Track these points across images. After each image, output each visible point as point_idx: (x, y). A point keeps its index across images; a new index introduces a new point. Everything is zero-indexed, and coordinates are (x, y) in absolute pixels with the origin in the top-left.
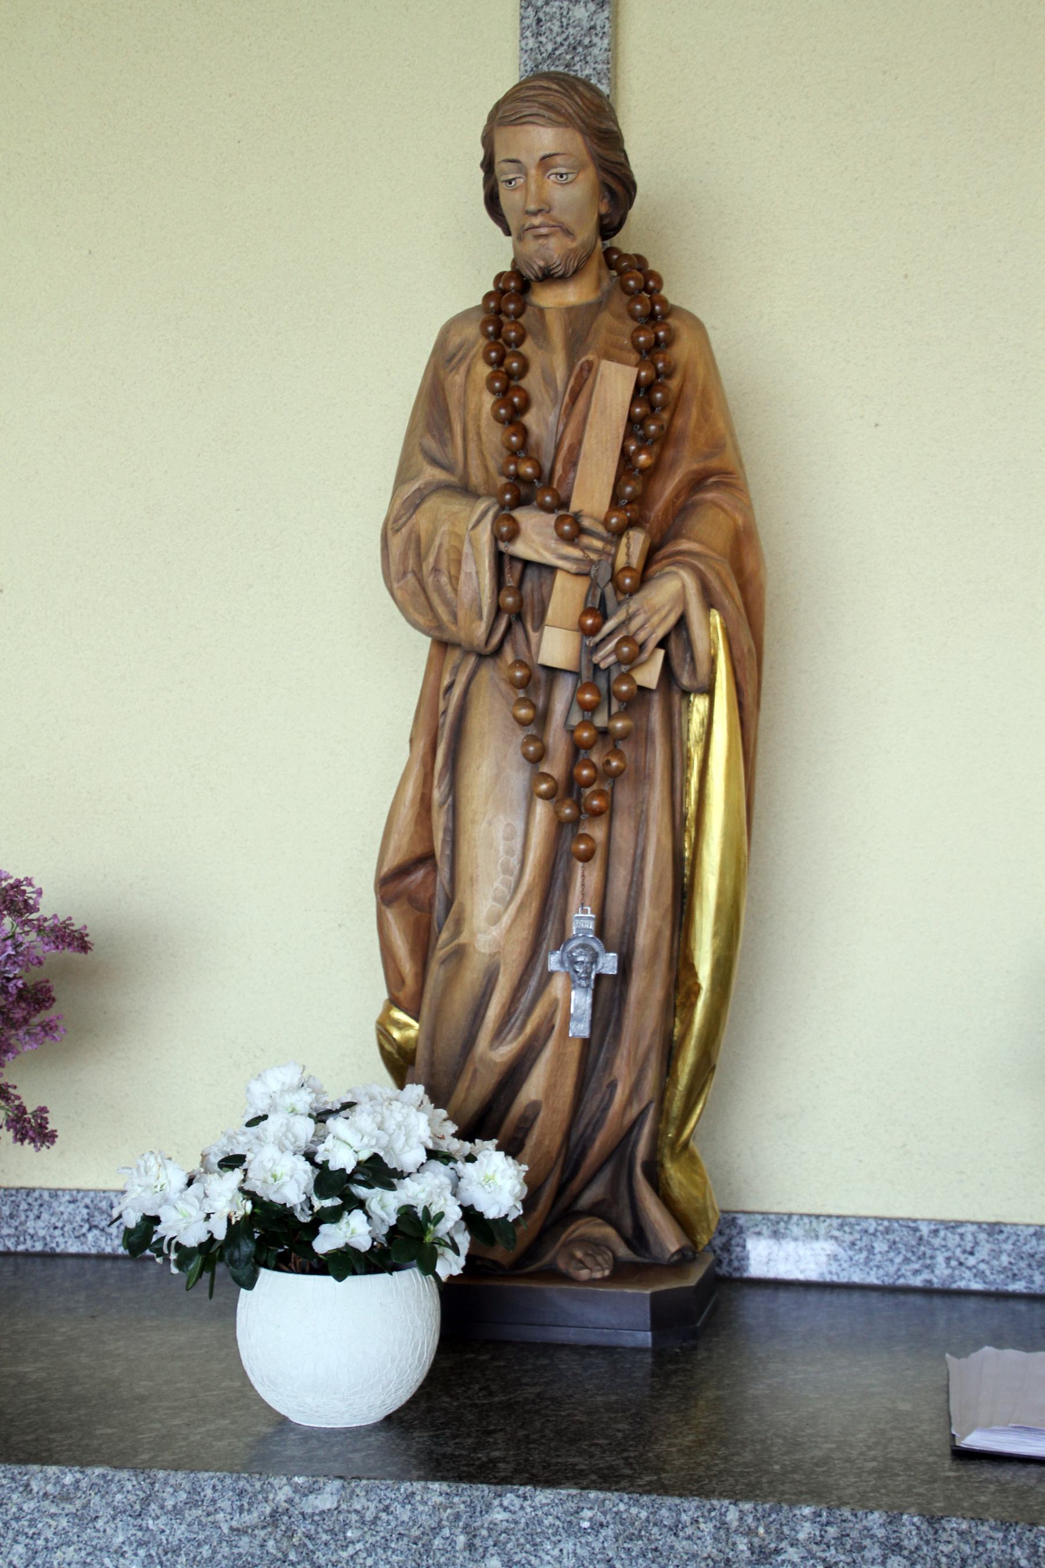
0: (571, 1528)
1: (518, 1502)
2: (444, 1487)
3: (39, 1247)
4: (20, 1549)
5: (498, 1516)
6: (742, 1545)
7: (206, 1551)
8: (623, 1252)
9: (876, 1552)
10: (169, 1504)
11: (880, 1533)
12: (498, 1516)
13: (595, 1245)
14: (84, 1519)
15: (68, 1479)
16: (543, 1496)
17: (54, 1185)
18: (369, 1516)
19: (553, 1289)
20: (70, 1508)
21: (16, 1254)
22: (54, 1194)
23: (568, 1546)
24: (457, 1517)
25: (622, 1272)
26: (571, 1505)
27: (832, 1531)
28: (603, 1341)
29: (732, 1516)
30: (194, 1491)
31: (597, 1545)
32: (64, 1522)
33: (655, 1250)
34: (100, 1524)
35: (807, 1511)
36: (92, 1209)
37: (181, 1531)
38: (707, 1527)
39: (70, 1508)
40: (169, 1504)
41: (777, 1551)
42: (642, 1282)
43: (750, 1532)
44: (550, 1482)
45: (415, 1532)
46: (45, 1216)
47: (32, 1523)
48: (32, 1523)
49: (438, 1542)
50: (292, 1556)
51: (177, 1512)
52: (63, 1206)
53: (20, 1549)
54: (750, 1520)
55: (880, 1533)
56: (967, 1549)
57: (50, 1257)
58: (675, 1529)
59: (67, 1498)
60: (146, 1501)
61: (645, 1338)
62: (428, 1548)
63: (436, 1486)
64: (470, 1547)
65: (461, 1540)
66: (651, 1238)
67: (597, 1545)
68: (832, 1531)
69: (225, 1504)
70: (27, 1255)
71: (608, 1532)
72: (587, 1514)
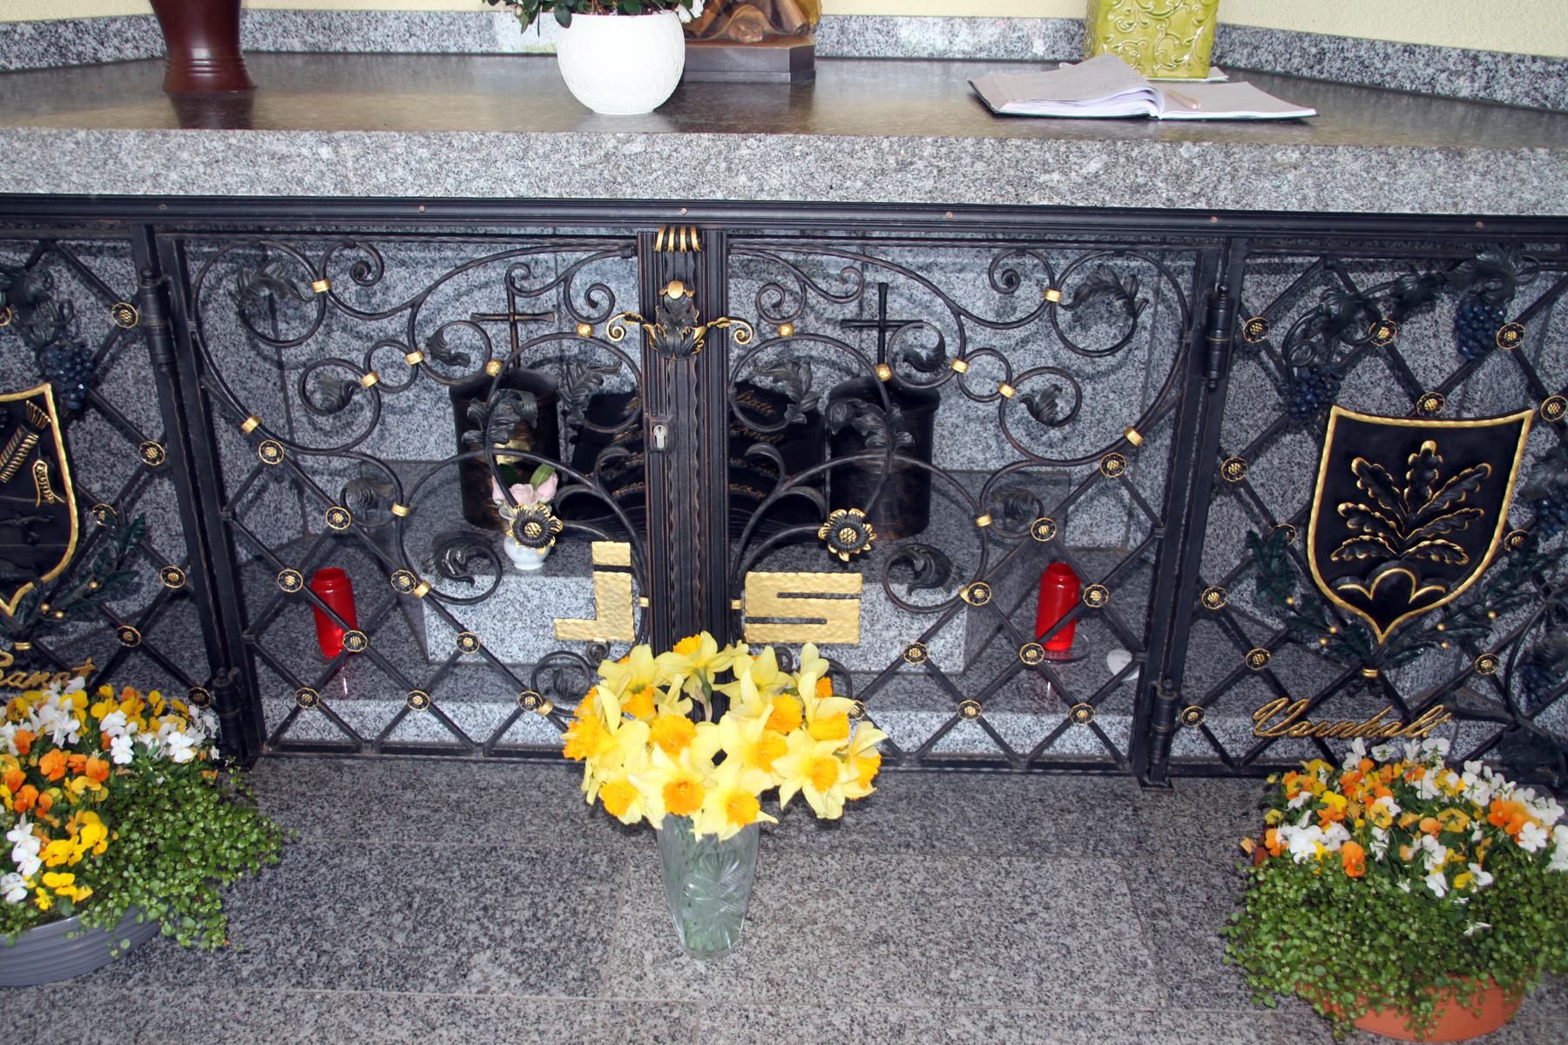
0: (789, 157)
1: (755, 143)
2: (711, 136)
3: (379, 49)
4: (450, 180)
5: (744, 152)
6: (892, 160)
7: (565, 179)
8: (768, 28)
9: (969, 160)
10: (541, 152)
11: (971, 150)
12: (744, 152)
13: (751, 23)
14: (488, 162)
15: (476, 139)
16: (771, 139)
17: (383, 8)
18: (665, 154)
19: (729, 50)
20: (479, 156)
21: (365, 54)
22: (384, 14)
23: (786, 168)
24: (720, 153)
25: (769, 39)
26: (789, 143)
27: (944, 150)
28: (761, 79)
29: (885, 144)
30: (555, 144)
31: (804, 166)
32: (476, 164)
33: (786, 26)
34: (499, 164)
35: (929, 140)
36: (410, 23)
37: (549, 168)
38: (870, 152)
39: (479, 156)
40: (541, 152)
41: (911, 163)
42: (786, 44)
43: (896, 153)
44: (774, 130)
45: (694, 163)
46: (380, 28)
47: (456, 165)
48: (456, 165)
49: (708, 168)
50: (620, 180)
51: (546, 156)
52: (390, 22)
53: (450, 180)
54: (896, 146)
55: (971, 150)
56: (1019, 155)
57: (387, 54)
58: (851, 154)
59: (476, 150)
60: (526, 151)
61: (787, 77)
62: (702, 172)
63: (705, 135)
64: (729, 169)
65: (723, 165)
66: (784, 18)
67: (804, 166)
68: (944, 150)
69: (575, 151)
70: (372, 54)
71: (811, 158)
72: (798, 148)
